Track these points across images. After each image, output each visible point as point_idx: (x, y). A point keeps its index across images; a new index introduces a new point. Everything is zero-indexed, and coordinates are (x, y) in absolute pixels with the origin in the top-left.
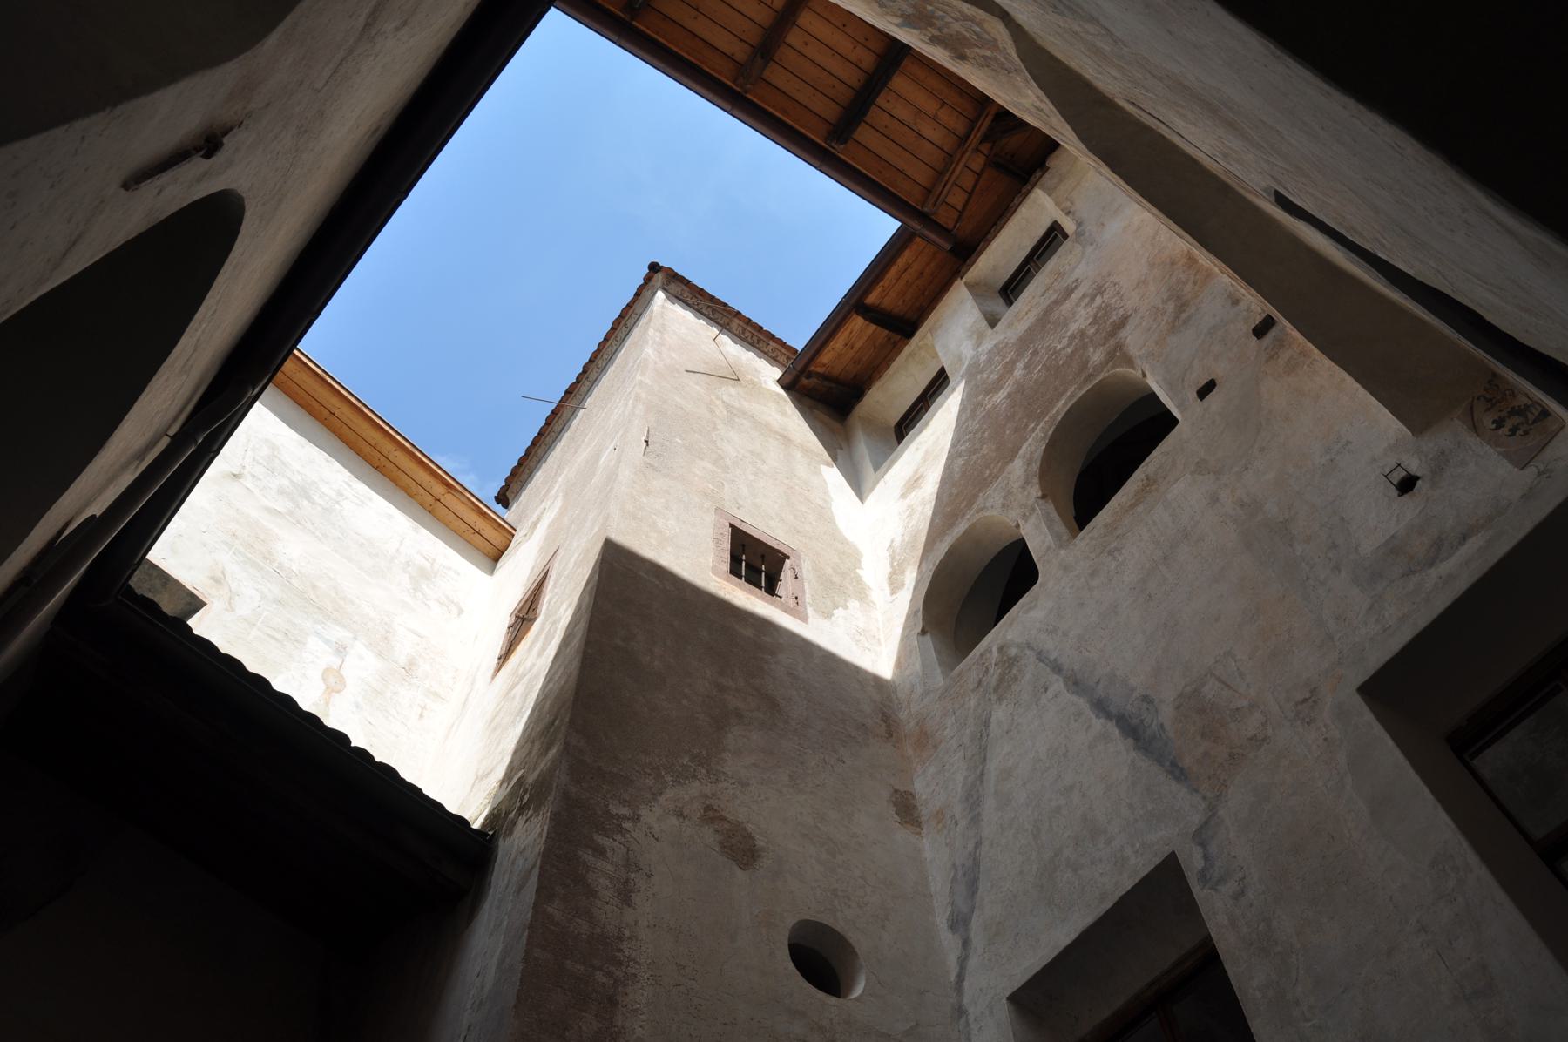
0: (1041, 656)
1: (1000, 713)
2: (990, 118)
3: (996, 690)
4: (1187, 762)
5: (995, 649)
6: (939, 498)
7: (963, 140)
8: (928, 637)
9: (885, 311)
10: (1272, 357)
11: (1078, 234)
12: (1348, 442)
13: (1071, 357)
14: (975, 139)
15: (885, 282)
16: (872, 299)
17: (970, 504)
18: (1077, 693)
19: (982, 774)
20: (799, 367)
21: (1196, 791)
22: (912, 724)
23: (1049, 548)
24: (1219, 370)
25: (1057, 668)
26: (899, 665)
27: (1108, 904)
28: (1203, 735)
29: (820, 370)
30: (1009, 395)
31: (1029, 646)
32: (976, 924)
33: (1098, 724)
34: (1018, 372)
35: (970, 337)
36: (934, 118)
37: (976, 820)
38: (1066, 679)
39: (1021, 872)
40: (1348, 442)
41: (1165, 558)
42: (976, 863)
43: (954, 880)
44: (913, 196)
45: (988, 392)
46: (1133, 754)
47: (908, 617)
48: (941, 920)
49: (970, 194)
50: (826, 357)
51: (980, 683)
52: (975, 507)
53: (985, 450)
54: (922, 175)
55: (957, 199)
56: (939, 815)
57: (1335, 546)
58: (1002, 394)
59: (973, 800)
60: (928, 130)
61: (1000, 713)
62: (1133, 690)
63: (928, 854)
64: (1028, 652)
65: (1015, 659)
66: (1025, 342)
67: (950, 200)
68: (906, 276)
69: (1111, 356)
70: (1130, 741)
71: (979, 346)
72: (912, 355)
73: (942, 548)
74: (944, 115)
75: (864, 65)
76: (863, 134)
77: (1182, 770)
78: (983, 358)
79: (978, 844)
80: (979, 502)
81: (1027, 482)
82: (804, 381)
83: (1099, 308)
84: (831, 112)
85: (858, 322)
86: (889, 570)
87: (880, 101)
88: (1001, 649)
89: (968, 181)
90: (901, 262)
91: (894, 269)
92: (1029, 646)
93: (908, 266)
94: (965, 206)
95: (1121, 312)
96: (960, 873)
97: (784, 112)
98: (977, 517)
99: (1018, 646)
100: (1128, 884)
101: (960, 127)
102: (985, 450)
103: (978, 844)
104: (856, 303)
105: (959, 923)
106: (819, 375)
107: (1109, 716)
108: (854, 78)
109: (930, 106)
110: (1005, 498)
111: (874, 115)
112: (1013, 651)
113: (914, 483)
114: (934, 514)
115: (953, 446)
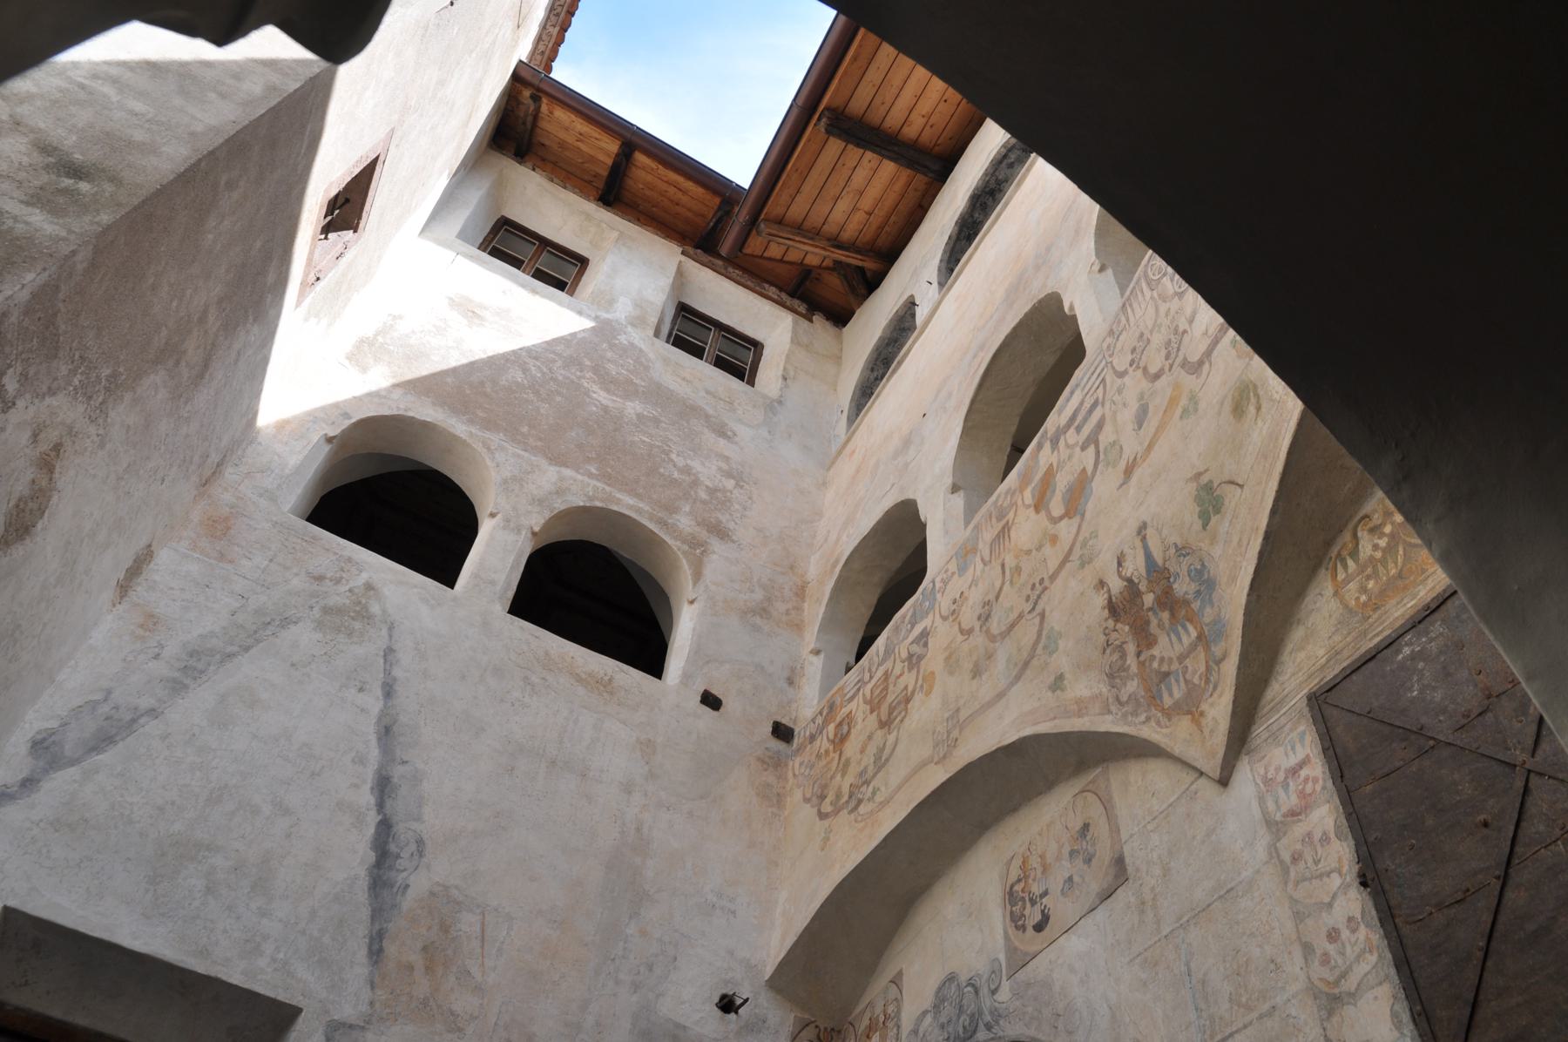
0: (389, 652)
1: (304, 636)
2: (860, 264)
3: (326, 610)
4: (391, 948)
5: (364, 576)
6: (472, 366)
7: (836, 243)
8: (327, 448)
9: (630, 174)
10: (763, 762)
11: (773, 406)
12: (734, 913)
13: (674, 483)
14: (839, 255)
15: (662, 170)
16: (640, 158)
17: (489, 424)
18: (379, 739)
19: (230, 656)
20: (543, 86)
21: (373, 988)
22: (227, 497)
23: (493, 583)
24: (730, 704)
25: (388, 692)
26: (281, 426)
27: (200, 967)
28: (425, 949)
29: (544, 108)
30: (606, 409)
31: (391, 628)
32: (60, 782)
33: (366, 798)
34: (633, 408)
35: (636, 305)
36: (855, 209)
37: (177, 687)
38: (383, 714)
39: (161, 809)
40: (734, 913)
41: (553, 762)
42: (131, 725)
43: (93, 705)
44: (774, 207)
45: (596, 369)
46: (362, 873)
47: (336, 405)
48: (35, 721)
49: (781, 261)
50: (560, 114)
51: (320, 579)
52: (488, 435)
53: (544, 408)
54: (796, 211)
55: (775, 251)
56: (151, 622)
57: (650, 968)
58: (601, 396)
59: (196, 665)
60: (843, 206)
61: (304, 636)
62: (419, 819)
63: (98, 636)
64: (384, 632)
65: (363, 615)
66: (657, 394)
67: (773, 246)
68: (672, 190)
69: (694, 543)
70: (372, 857)
71: (633, 325)
72: (588, 217)
73: (425, 411)
74: (859, 217)
75: (906, 130)
76: (835, 145)
77: (381, 950)
78: (623, 339)
79: (153, 713)
80: (495, 438)
81: (540, 502)
82: (527, 93)
83: (724, 491)
84: (857, 106)
85: (613, 147)
86: (370, 334)
87: (869, 155)
88: (369, 587)
89: (793, 256)
90: (689, 185)
91: (680, 179)
92: (391, 628)
93: (684, 192)
94: (770, 259)
95: (731, 525)
96: (105, 709)
97: (855, 59)
98: (478, 447)
99: (384, 611)
100: (236, 978)
101: (847, 235)
102: (544, 408)
103: (153, 713)
104: (633, 142)
105: (48, 753)
106: (538, 110)
107: (380, 806)
108: (893, 122)
109: (866, 203)
110: (514, 478)
111: (854, 152)
112: (375, 608)
113: (471, 311)
114: (454, 370)
115: (528, 351)
